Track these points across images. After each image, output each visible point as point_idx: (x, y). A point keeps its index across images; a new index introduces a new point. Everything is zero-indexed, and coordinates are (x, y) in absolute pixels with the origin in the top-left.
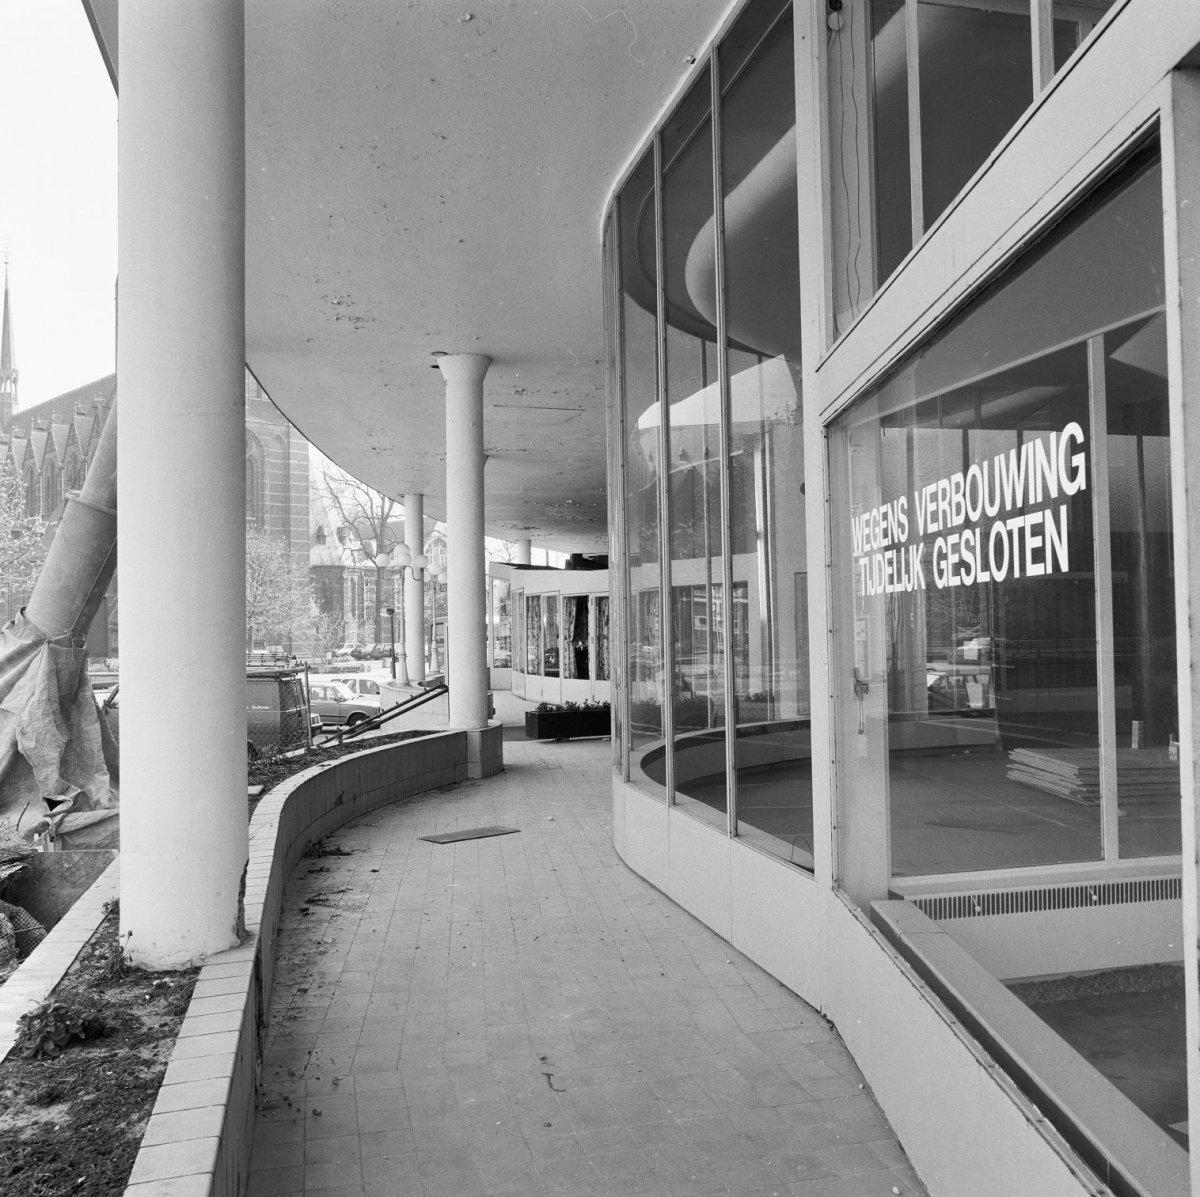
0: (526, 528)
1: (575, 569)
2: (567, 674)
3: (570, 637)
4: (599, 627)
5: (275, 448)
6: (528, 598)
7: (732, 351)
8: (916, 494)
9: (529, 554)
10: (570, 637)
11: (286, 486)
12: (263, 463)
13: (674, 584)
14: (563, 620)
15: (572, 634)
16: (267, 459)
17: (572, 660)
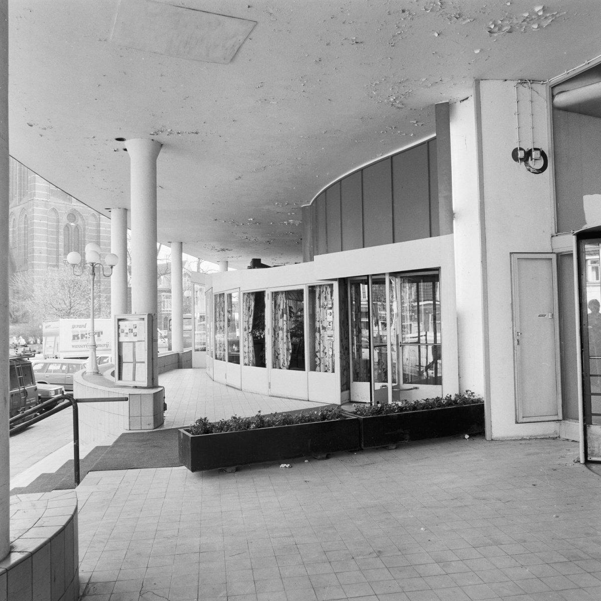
0: (223, 250)
1: (254, 268)
2: (247, 362)
3: (249, 328)
4: (275, 320)
5: (92, 221)
6: (215, 296)
7: (361, 172)
8: (284, 307)
9: (181, 256)
10: (249, 328)
11: (98, 242)
12: (85, 229)
13: (145, 384)
14: (241, 316)
15: (251, 327)
16: (87, 227)
17: (251, 349)
